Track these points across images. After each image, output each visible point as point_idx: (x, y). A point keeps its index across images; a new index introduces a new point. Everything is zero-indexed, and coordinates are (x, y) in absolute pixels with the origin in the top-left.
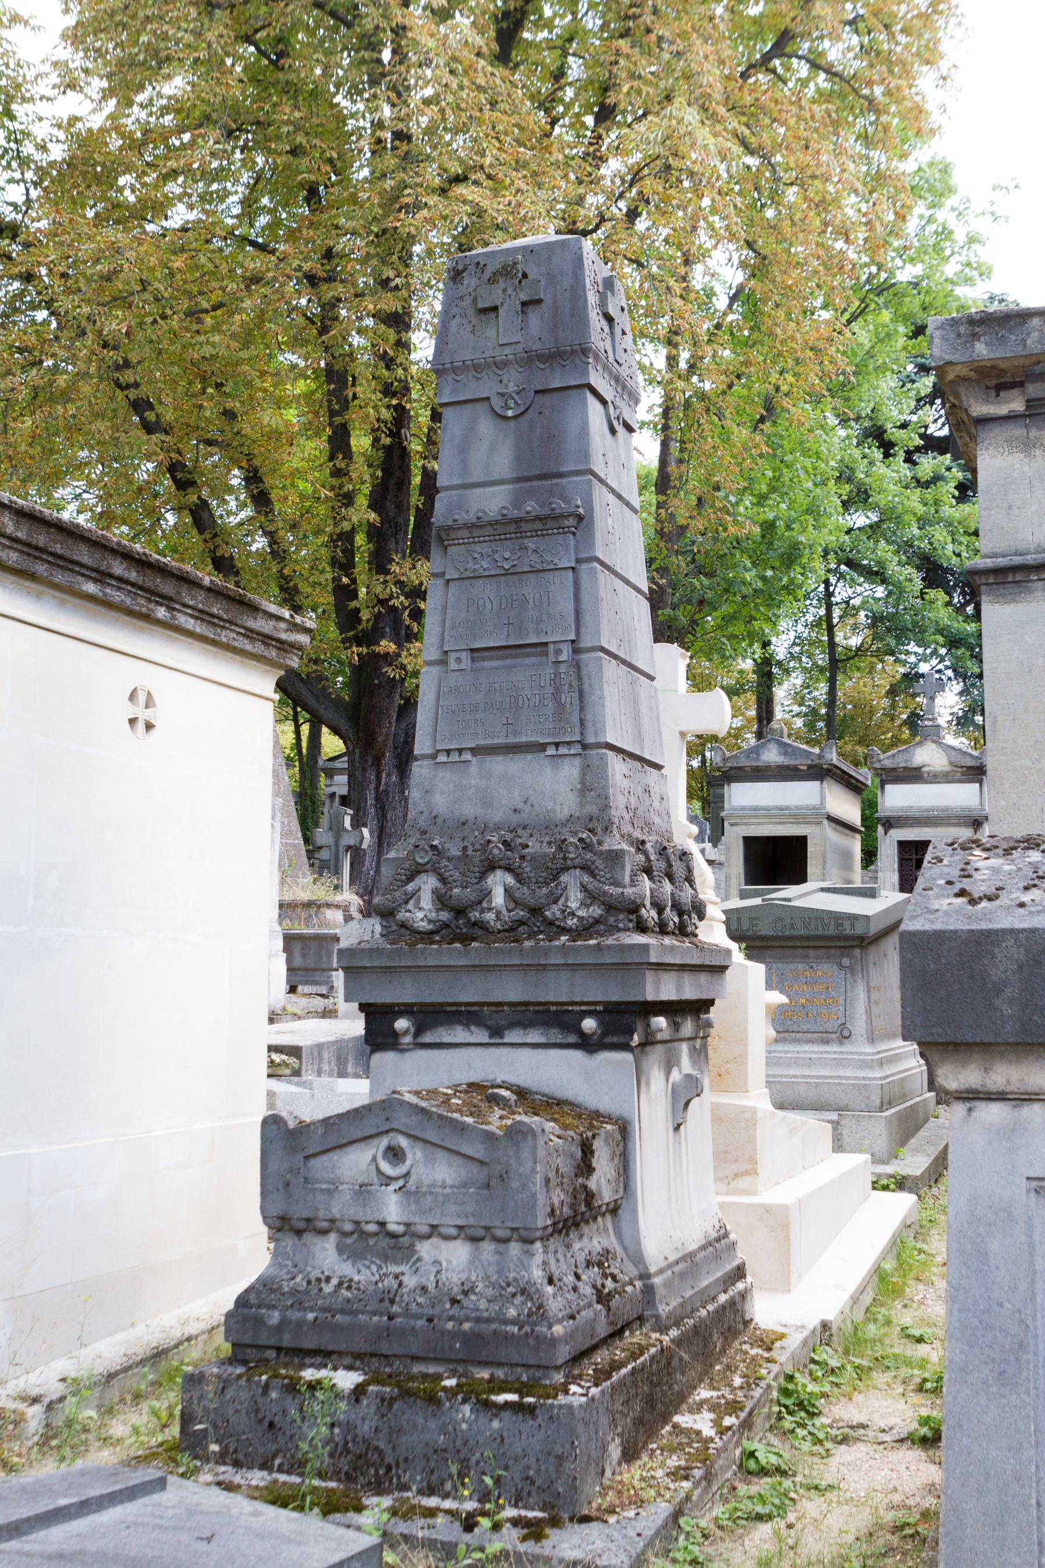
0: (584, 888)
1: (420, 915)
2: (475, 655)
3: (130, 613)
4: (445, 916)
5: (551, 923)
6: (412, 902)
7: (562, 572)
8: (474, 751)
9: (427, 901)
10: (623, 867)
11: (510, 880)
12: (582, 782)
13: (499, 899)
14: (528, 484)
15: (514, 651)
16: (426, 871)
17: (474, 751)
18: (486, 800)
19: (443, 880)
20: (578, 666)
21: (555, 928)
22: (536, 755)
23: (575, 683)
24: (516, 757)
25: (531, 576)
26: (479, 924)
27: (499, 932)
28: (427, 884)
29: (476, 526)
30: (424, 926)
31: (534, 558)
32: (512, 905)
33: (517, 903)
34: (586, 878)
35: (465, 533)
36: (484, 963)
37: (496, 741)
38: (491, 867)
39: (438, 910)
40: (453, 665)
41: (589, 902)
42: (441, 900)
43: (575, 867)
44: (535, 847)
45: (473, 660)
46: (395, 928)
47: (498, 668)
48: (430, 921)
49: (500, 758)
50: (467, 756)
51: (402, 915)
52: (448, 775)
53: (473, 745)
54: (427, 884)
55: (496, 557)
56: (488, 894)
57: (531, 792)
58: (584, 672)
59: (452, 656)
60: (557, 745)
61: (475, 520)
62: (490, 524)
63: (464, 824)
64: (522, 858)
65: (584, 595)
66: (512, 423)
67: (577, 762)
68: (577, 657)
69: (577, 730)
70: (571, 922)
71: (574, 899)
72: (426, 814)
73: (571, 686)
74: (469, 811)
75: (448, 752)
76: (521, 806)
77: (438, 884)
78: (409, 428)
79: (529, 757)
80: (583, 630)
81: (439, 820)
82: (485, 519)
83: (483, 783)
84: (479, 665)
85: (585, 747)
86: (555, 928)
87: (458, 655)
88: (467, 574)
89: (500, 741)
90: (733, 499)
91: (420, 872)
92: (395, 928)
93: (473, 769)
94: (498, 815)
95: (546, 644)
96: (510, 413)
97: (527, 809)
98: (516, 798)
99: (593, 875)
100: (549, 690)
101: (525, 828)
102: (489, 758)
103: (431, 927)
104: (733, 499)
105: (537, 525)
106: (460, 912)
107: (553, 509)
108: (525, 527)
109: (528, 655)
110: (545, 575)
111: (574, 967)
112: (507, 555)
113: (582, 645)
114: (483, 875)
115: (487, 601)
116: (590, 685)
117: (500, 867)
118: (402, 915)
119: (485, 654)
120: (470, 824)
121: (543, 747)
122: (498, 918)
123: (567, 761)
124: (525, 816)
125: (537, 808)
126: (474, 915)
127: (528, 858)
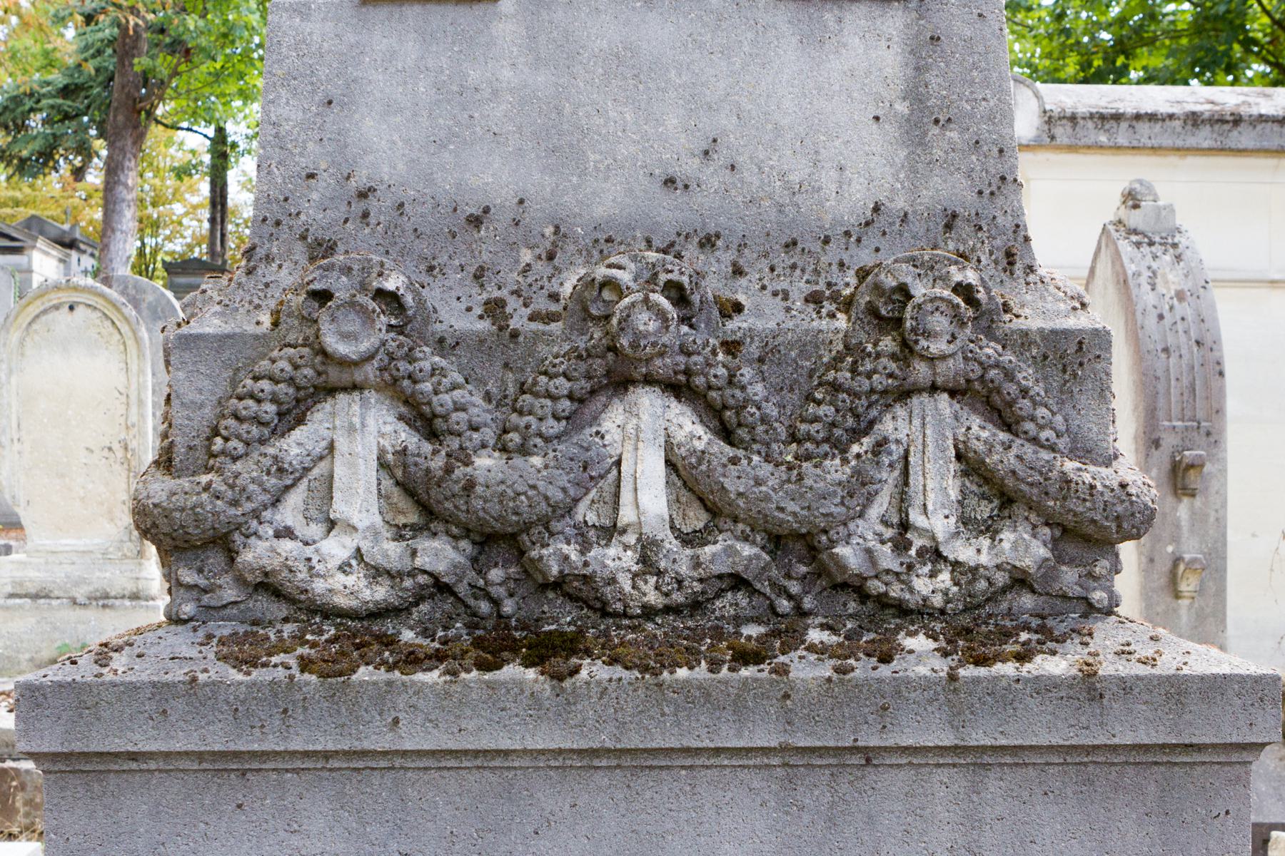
0: (969, 464)
1: (336, 548)
3: (1177, 150)
4: (439, 554)
5: (856, 587)
6: (295, 499)
9: (360, 498)
10: (1104, 393)
11: (688, 427)
12: (916, 95)
13: (649, 498)
16: (355, 387)
18: (560, 143)
19: (427, 423)
21: (879, 614)
26: (581, 590)
27: (649, 612)
28: (360, 436)
30: (351, 589)
32: (697, 519)
33: (713, 511)
34: (980, 431)
36: (633, 741)
38: (619, 376)
39: (541, 558)
41: (984, 510)
42: (421, 499)
43: (934, 389)
44: (762, 316)
46: (230, 593)
48: (377, 573)
51: (258, 553)
52: (410, 50)
54: (360, 436)
56: (602, 475)
57: (726, 121)
63: (475, 221)
64: (731, 347)
70: (930, 586)
71: (938, 503)
72: (326, 181)
74: (493, 176)
76: (689, 167)
77: (409, 438)
81: (380, 207)
83: (542, 78)
86: (879, 614)
91: (331, 391)
92: (230, 593)
94: (607, 197)
97: (713, 177)
98: (675, 143)
99: (1004, 417)
101: (708, 242)
103: (380, 593)
106: (496, 539)
111: (973, 759)
114: (581, 409)
117: (649, 381)
118: (258, 553)
120: (500, 221)
122: (647, 562)
124: (710, 201)
125: (749, 174)
126: (558, 554)
127: (753, 349)
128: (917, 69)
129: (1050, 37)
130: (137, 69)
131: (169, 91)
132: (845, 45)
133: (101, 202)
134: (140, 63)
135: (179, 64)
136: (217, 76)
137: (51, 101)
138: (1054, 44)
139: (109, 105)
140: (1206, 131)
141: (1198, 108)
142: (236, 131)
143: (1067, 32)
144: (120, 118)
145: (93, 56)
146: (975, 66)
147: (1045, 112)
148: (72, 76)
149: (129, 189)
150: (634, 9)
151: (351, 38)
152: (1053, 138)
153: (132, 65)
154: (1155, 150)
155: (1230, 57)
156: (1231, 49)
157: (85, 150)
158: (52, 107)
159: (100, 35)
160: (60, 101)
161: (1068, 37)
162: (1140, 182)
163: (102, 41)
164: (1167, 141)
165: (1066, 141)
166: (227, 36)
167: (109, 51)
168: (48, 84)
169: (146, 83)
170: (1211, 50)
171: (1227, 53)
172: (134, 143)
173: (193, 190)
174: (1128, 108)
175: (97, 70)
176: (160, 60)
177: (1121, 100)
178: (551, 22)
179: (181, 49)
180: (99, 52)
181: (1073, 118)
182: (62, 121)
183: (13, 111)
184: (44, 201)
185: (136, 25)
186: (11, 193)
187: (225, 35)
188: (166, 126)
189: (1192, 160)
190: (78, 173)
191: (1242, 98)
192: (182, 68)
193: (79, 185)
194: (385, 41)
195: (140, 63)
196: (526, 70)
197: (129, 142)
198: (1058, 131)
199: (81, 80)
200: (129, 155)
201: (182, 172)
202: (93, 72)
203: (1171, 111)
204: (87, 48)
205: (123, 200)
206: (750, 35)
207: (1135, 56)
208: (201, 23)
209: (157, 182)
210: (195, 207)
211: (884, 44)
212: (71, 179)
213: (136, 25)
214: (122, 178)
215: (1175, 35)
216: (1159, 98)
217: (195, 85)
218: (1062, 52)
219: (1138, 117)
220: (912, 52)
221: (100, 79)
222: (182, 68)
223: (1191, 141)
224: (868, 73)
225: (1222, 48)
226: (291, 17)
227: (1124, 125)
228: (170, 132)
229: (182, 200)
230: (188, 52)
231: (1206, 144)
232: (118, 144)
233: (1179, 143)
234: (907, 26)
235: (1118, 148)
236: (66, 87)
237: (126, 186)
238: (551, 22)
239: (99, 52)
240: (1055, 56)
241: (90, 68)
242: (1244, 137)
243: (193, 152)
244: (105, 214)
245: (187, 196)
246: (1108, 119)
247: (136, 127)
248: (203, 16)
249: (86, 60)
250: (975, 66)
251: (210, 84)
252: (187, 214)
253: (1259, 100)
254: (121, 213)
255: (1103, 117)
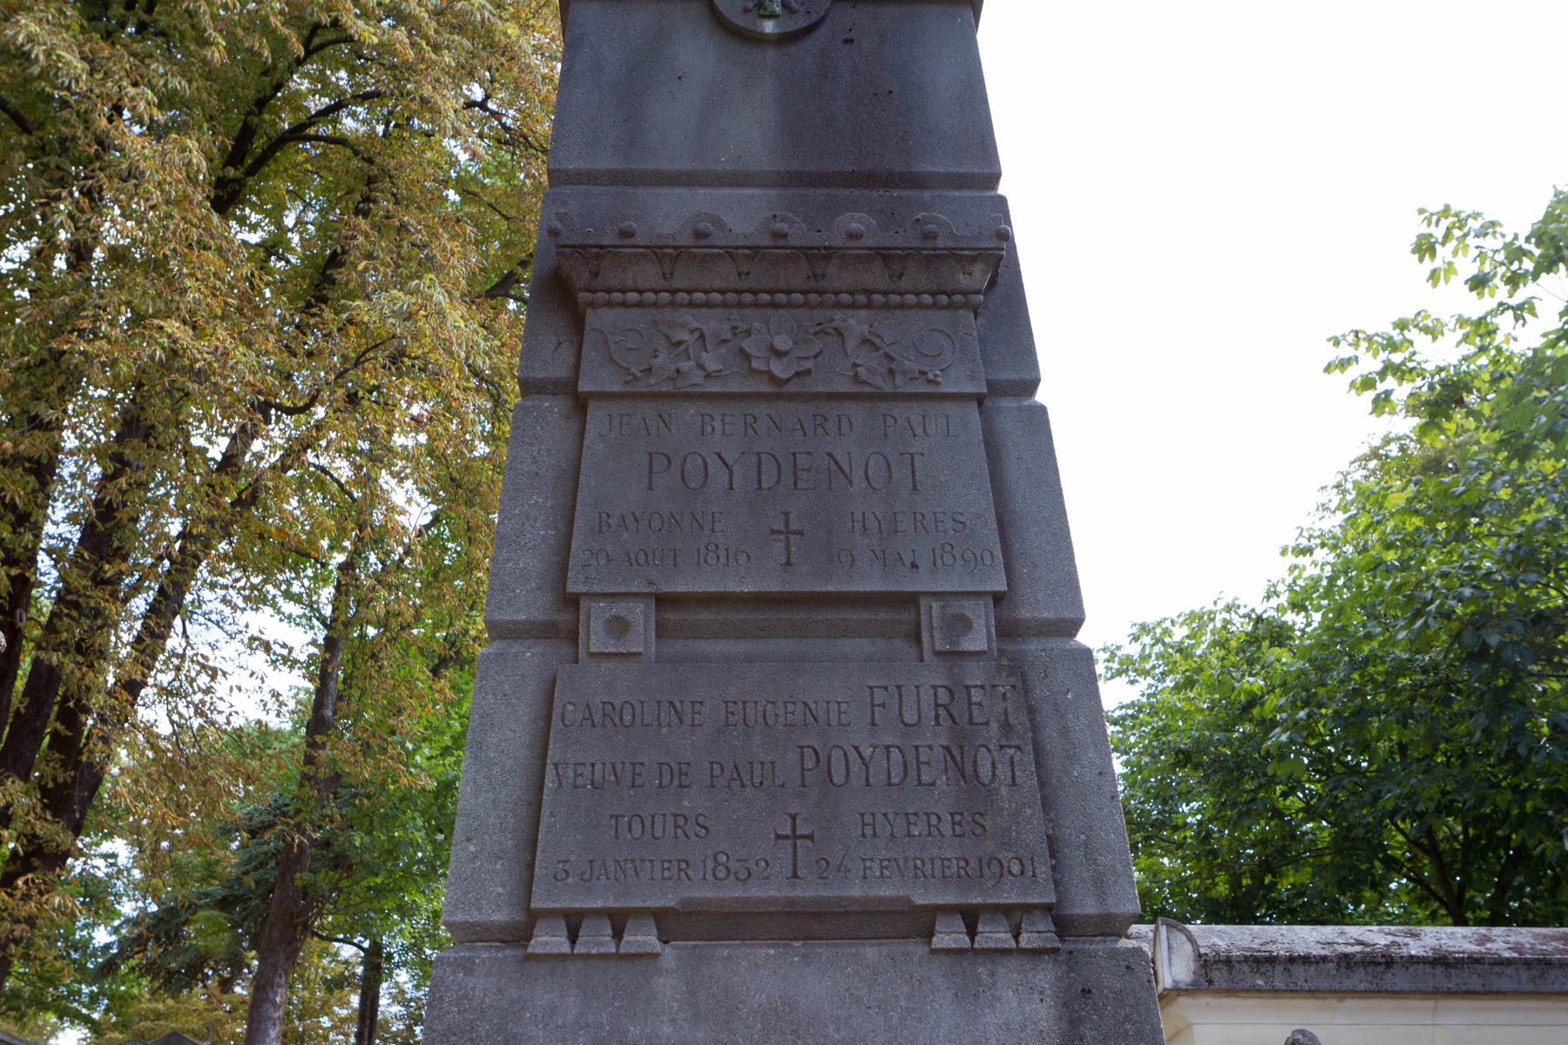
2: (670, 616)
7: (952, 409)
8: (669, 923)
14: (821, 192)
15: (799, 615)
17: (669, 923)
20: (1017, 669)
22: (896, 947)
23: (1019, 720)
24: (823, 951)
25: (856, 411)
29: (695, 250)
31: (869, 362)
35: (649, 274)
37: (755, 891)
40: (597, 639)
45: (662, 631)
47: (749, 659)
49: (765, 952)
50: (643, 938)
53: (669, 901)
55: (746, 344)
58: (1040, 692)
59: (596, 619)
60: (971, 918)
61: (686, 240)
62: (731, 253)
65: (1014, 472)
66: (770, 54)
67: (1045, 976)
68: (1010, 647)
69: (1043, 872)
73: (1006, 727)
75: (573, 923)
78: (27, 611)
79: (871, 952)
80: (1023, 571)
82: (719, 239)
84: (678, 647)
85: (1064, 926)
87: (619, 609)
88: (653, 384)
89: (770, 891)
90: (410, 746)
93: (667, 985)
95: (911, 600)
96: (769, 27)
100: (935, 738)
102: (724, 950)
104: (410, 746)
105: (875, 276)
107: (932, 236)
108: (838, 277)
109: (846, 632)
110: (899, 410)
112: (782, 343)
113: (1025, 613)
115: (715, 467)
116: (1065, 732)
119: (704, 615)
121: (922, 923)
123: (1009, 971)
128: (1071, 1022)
129: (1197, 857)
130: (298, 883)
131: (328, 906)
132: (999, 999)
133: (246, 1015)
134: (301, 878)
135: (340, 879)
136: (380, 891)
137: (207, 913)
138: (1203, 864)
139: (265, 919)
140: (1360, 973)
141: (1350, 950)
142: (394, 944)
143: (1214, 853)
144: (276, 933)
145: (256, 869)
146: (1127, 1018)
147: (1200, 955)
148: (232, 887)
149: (276, 1007)
150: (792, 963)
151: (513, 993)
152: (1210, 982)
153: (293, 879)
154: (1313, 993)
155: (1372, 875)
156: (1373, 867)
157: (237, 963)
158: (208, 918)
159: (265, 848)
160: (216, 913)
161: (1216, 858)
162: (1302, 1032)
163: (266, 853)
164: (1323, 984)
165: (1224, 985)
166: (392, 851)
167: (272, 863)
168: (206, 895)
169: (305, 895)
170: (1353, 869)
171: (1369, 872)
172: (287, 959)
173: (344, 1003)
174: (1280, 950)
175: (258, 883)
176: (322, 876)
177: (1274, 942)
178: (711, 977)
179: (341, 863)
180: (262, 865)
181: (1228, 962)
182: (216, 933)
183: (169, 922)
184: (188, 1013)
185: (301, 845)
186: (153, 1005)
187: (390, 852)
188: (321, 937)
189: (1350, 1003)
190: (226, 986)
191: (1390, 938)
192: (344, 883)
193: (225, 997)
194: (547, 996)
195: (301, 878)
196: (686, 1026)
197: (282, 958)
198: (1215, 975)
199: (241, 892)
200: (280, 971)
201: (337, 984)
202: (253, 886)
203: (1323, 953)
204: (250, 860)
205: (270, 1018)
206: (905, 989)
207: (1282, 875)
208: (367, 840)
209: (306, 994)
210: (343, 1021)
211: (1037, 997)
212: (217, 992)
213: (301, 845)
214: (271, 995)
215: (1319, 854)
216: (1306, 938)
217: (355, 900)
218: (1210, 871)
219: (1292, 959)
220: (1065, 1005)
221: (260, 891)
222: (344, 883)
223: (1347, 984)
224: (1023, 1028)
225: (1364, 867)
226: (454, 973)
227: (1279, 968)
228: (325, 944)
229: (330, 1014)
230: (350, 866)
231: (1362, 987)
232: (270, 960)
233: (1336, 986)
234: (1059, 979)
235: (1275, 992)
236: (224, 899)
237: (274, 1003)
238: (711, 977)
239: (262, 865)
240: (1204, 875)
241: (250, 881)
242: (1399, 979)
243: (346, 962)
244: (249, 1031)
245: (336, 1009)
246: (1262, 962)
247: (290, 943)
248: (369, 833)
249: (245, 874)
250: (1127, 1018)
251: (370, 900)
252: (333, 1028)
253: (1407, 940)
254: (266, 1033)
255: (1257, 960)
